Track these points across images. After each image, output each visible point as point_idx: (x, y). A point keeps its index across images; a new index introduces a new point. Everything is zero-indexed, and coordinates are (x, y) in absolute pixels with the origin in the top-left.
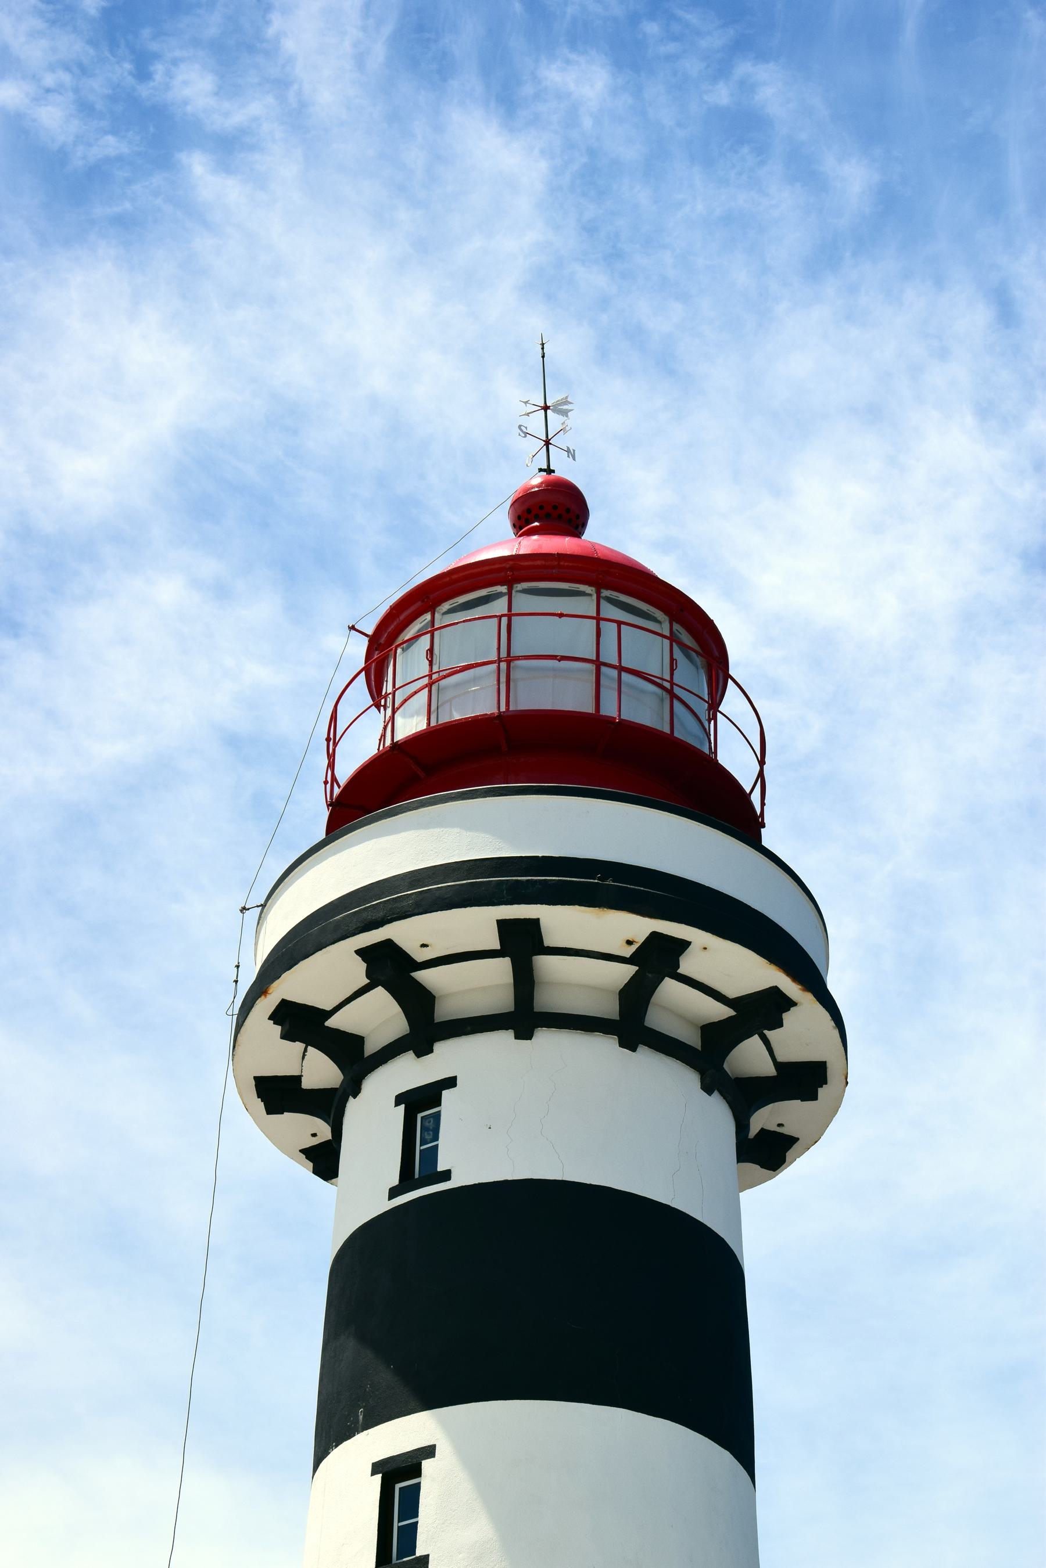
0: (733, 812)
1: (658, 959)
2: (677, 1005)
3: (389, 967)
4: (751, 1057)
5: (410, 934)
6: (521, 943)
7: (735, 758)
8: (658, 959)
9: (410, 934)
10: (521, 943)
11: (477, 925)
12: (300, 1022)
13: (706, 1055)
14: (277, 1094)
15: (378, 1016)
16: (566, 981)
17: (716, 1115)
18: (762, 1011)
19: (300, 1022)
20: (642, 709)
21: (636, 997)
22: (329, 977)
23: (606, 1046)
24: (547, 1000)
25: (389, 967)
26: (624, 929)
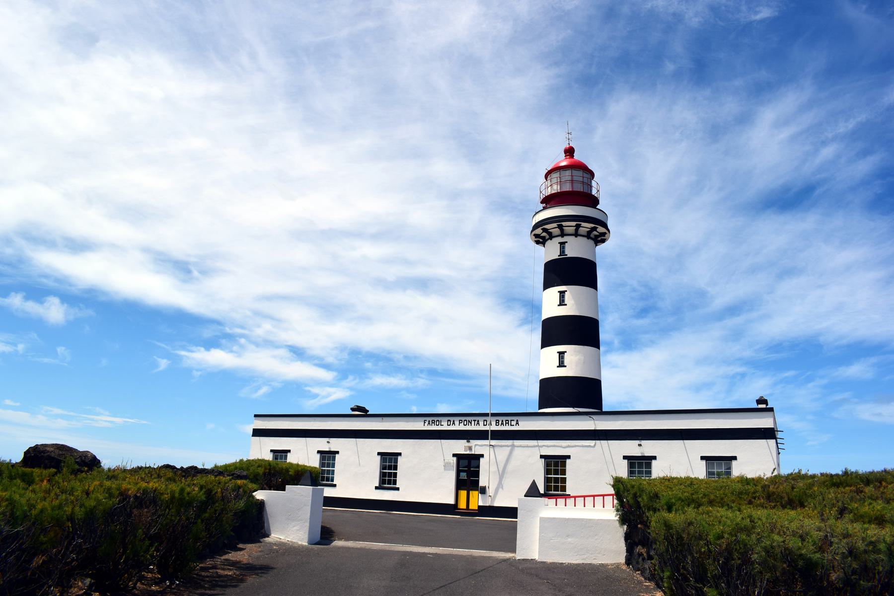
0: (593, 202)
1: (578, 226)
2: (582, 230)
3: (545, 230)
4: (595, 233)
5: (547, 227)
6: (560, 227)
7: (594, 192)
8: (578, 226)
9: (547, 227)
10: (560, 227)
11: (555, 225)
12: (536, 236)
13: (588, 236)
14: (538, 242)
15: (544, 234)
16: (568, 230)
17: (591, 242)
18: (594, 229)
19: (536, 236)
20: (579, 188)
21: (577, 230)
22: (539, 231)
23: (573, 237)
24: (565, 232)
25: (545, 230)
26: (574, 223)
